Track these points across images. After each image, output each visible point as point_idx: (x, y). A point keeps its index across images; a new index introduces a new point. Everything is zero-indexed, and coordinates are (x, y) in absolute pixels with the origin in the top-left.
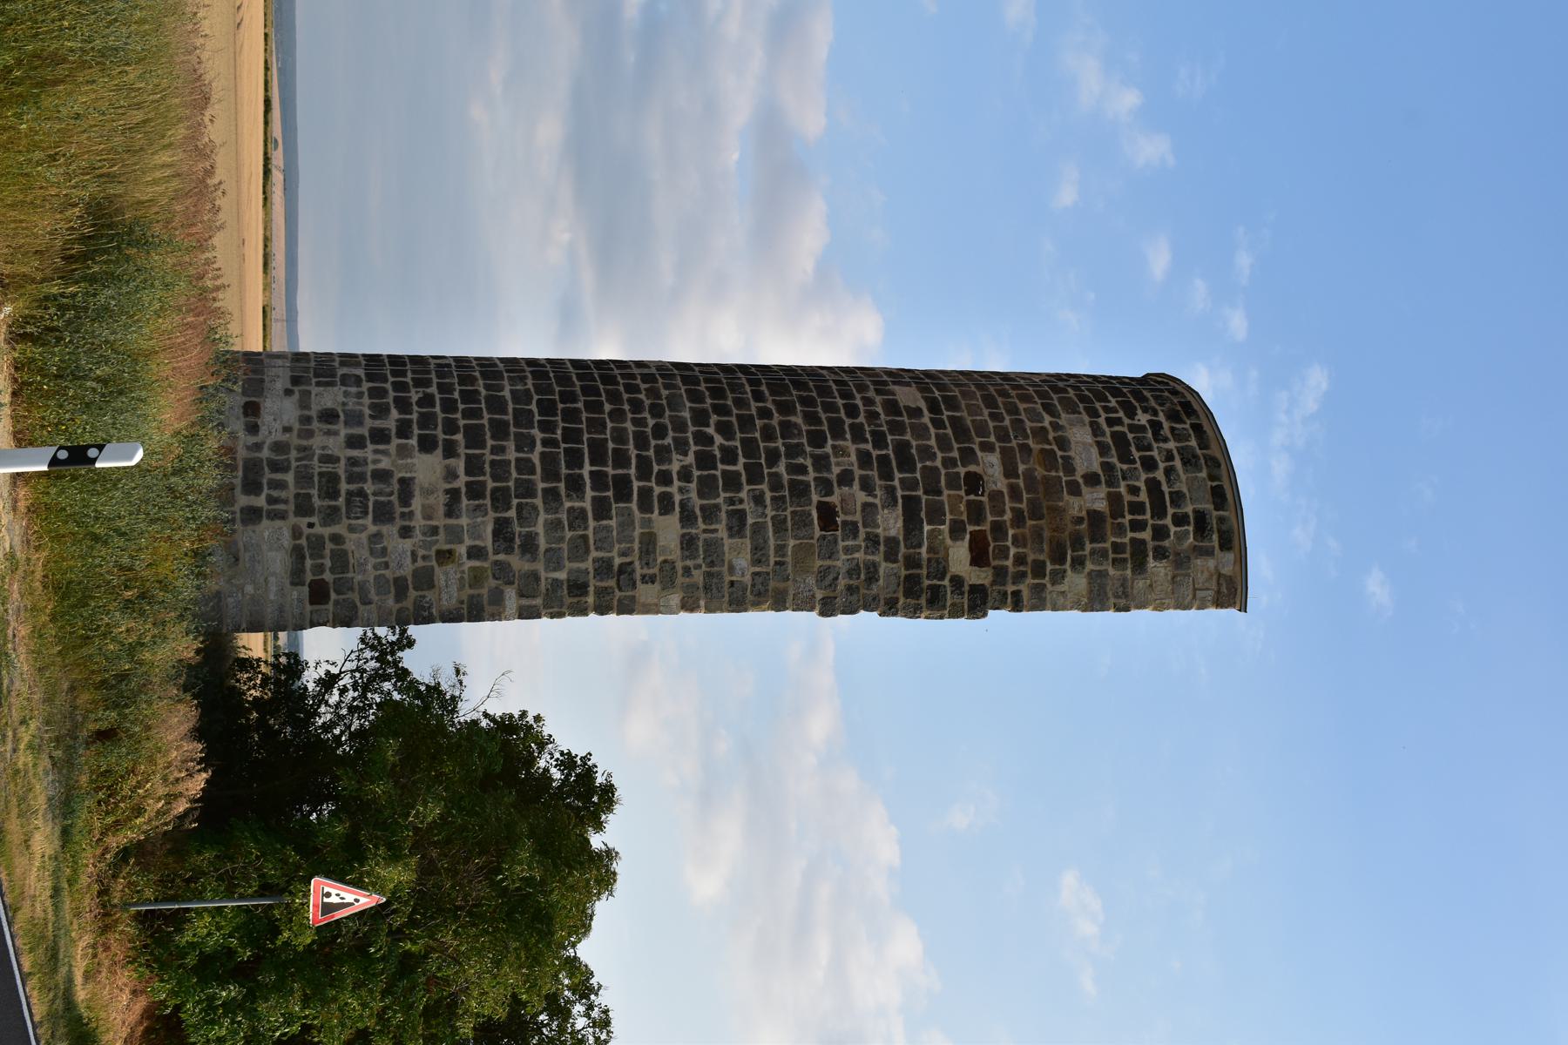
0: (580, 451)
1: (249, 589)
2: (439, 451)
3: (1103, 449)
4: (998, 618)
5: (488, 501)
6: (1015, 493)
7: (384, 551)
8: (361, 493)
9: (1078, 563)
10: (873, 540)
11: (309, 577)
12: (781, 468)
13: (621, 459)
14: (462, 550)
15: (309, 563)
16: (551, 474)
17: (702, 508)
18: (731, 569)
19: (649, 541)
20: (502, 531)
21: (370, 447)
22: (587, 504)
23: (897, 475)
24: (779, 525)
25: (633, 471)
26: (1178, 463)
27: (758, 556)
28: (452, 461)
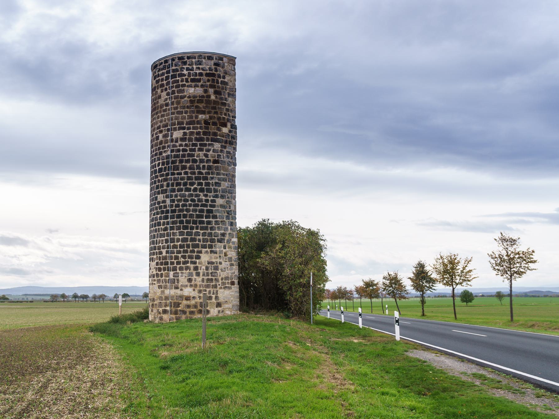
0: (174, 218)
1: (232, 299)
2: (200, 255)
3: (196, 86)
4: (237, 122)
5: (213, 244)
6: (209, 113)
7: (225, 268)
8: (211, 273)
9: (226, 99)
10: (221, 151)
11: (230, 285)
12: (204, 171)
13: (202, 211)
14: (224, 250)
15: (227, 285)
16: (206, 228)
17: (214, 192)
18: (228, 187)
19: (222, 206)
20: (220, 241)
21: (199, 271)
22: (214, 220)
23: (205, 142)
24: (218, 174)
25: (205, 208)
26: (200, 66)
27: (224, 180)
28: (203, 252)
